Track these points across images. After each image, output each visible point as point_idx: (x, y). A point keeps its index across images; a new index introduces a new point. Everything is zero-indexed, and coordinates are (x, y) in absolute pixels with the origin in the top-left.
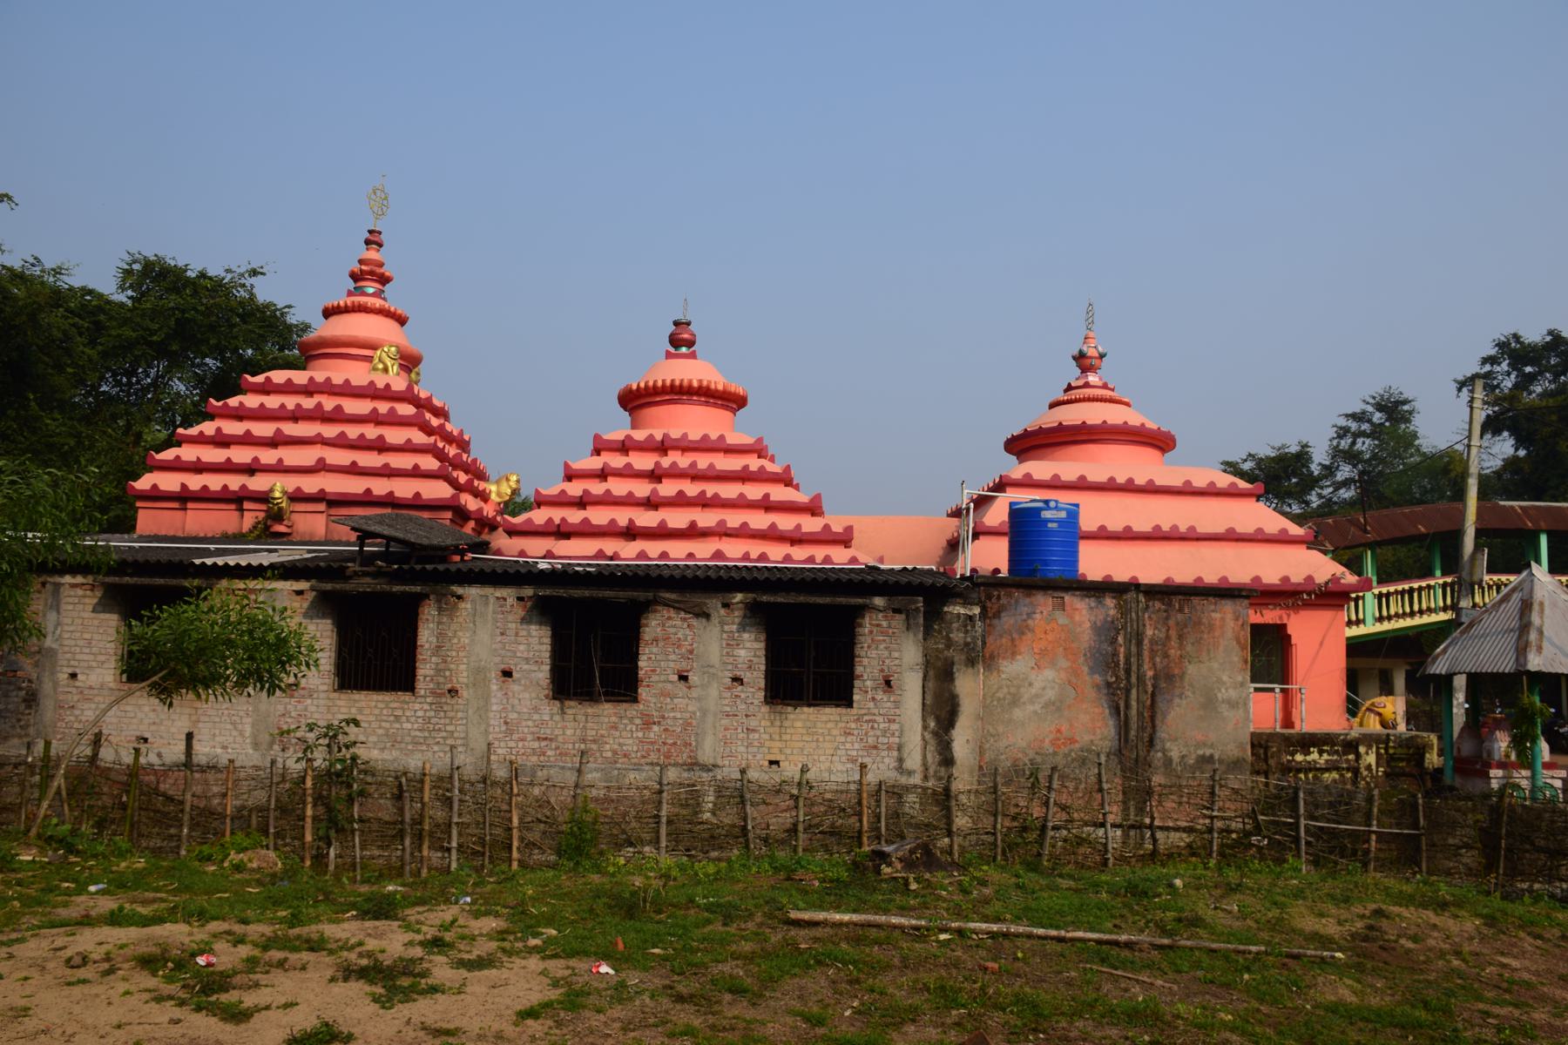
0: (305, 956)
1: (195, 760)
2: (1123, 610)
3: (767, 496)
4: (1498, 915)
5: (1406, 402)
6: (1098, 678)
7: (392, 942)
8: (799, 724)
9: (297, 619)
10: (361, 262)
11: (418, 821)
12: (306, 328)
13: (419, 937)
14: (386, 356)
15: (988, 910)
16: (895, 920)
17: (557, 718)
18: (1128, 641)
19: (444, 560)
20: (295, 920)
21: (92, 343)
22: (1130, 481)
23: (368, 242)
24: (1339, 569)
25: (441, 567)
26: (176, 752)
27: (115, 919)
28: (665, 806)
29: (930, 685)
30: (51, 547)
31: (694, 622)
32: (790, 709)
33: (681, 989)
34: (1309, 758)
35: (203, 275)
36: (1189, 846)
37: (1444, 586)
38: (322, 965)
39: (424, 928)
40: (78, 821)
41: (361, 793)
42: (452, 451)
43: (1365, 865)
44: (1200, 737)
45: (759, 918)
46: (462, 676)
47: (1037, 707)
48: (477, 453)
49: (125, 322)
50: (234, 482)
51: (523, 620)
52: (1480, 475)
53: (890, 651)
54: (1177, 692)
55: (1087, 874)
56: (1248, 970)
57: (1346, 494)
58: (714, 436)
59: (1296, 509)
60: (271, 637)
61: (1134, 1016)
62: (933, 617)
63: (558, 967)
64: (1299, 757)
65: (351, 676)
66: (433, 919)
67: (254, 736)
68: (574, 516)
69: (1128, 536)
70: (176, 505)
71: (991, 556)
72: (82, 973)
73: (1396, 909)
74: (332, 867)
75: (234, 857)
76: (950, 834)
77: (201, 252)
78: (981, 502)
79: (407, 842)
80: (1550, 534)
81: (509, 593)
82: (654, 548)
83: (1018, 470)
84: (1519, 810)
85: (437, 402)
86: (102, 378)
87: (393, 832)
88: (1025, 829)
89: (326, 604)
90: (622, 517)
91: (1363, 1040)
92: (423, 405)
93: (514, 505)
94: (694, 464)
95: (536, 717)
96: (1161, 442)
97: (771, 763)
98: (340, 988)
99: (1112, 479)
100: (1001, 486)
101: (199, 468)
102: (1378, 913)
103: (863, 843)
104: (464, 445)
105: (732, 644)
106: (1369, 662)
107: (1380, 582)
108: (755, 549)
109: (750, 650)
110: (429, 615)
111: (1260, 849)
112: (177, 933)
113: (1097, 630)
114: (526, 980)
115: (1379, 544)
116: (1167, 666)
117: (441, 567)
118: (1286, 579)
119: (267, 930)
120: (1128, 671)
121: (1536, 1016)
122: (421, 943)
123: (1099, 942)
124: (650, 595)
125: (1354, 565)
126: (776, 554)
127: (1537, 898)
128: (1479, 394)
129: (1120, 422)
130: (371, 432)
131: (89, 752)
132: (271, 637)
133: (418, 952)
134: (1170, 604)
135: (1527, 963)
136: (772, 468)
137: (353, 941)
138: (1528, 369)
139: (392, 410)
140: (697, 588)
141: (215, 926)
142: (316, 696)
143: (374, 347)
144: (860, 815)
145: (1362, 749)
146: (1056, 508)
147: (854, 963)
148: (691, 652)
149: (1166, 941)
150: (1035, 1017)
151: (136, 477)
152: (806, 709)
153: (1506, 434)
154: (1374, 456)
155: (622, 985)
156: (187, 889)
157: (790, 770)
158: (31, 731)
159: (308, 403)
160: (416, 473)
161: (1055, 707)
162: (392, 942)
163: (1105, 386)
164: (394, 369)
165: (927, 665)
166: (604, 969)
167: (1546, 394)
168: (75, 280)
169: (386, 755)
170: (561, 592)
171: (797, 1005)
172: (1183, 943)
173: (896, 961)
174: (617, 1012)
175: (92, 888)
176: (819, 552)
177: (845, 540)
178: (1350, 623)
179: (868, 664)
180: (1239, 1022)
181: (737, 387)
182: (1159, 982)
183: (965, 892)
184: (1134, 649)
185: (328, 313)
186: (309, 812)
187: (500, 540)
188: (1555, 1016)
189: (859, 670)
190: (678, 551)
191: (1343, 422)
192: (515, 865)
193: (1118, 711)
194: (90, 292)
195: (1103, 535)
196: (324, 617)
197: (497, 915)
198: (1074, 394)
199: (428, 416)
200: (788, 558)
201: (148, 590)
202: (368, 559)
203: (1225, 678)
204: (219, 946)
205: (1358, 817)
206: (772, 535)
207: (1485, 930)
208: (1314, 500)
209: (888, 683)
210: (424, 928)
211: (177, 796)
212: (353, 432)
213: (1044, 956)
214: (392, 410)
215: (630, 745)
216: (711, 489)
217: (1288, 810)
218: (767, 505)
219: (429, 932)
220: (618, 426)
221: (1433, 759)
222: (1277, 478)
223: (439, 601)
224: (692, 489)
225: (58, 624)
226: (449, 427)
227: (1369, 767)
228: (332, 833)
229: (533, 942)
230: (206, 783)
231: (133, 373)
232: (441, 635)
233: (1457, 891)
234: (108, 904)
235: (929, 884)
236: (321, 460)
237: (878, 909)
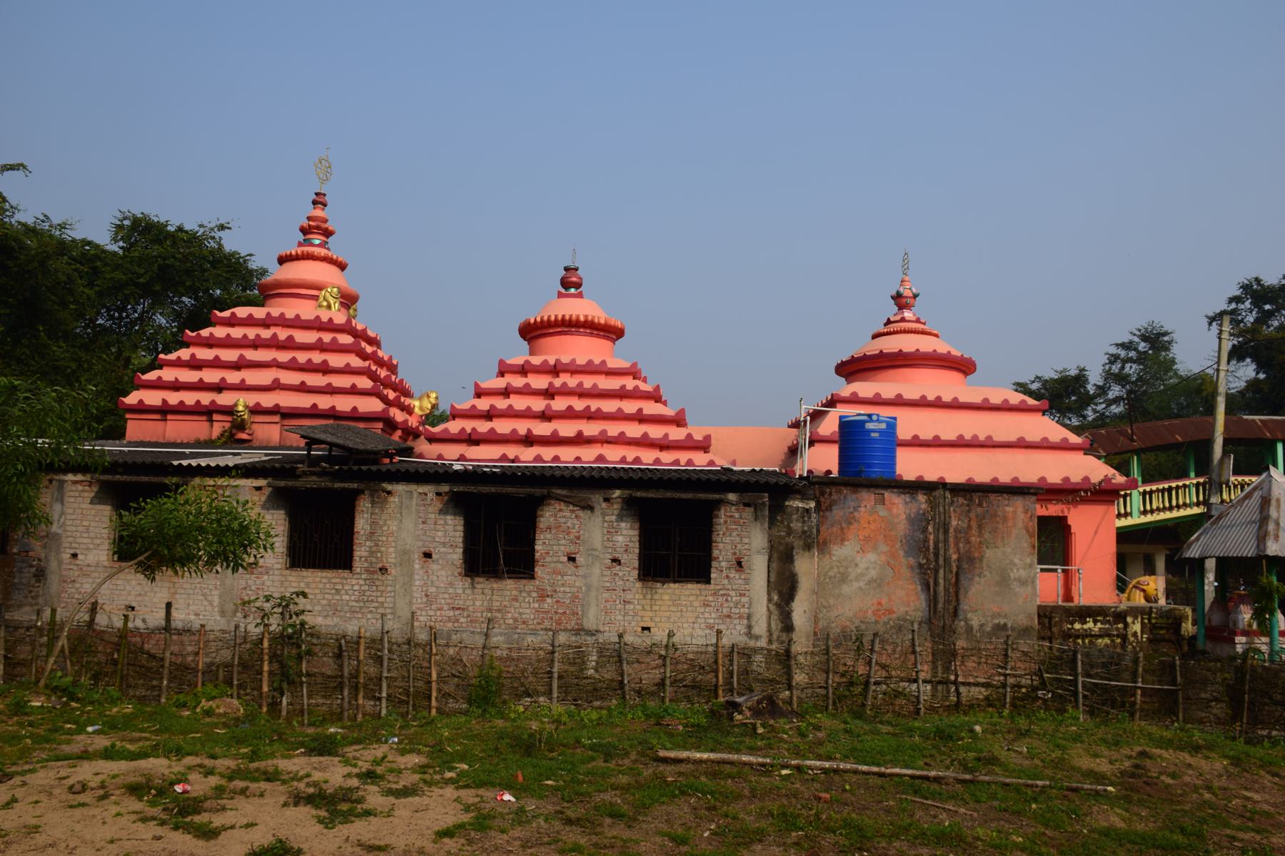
0: (263, 785)
1: (173, 625)
2: (933, 505)
3: (640, 410)
4: (1243, 756)
5: (1166, 334)
6: (912, 561)
7: (334, 774)
8: (666, 597)
10: (309, 218)
11: (355, 676)
12: (264, 272)
13: (356, 771)
14: (330, 295)
15: (822, 751)
16: (745, 758)
17: (468, 591)
18: (937, 530)
19: (376, 462)
20: (254, 756)
21: (91, 285)
22: (939, 398)
23: (315, 203)
24: (1110, 471)
25: (374, 468)
26: (157, 618)
27: (108, 754)
28: (556, 664)
29: (774, 565)
30: (57, 451)
31: (581, 513)
32: (659, 585)
33: (570, 813)
34: (1085, 627)
35: (180, 229)
36: (987, 698)
37: (1197, 485)
38: (277, 793)
39: (360, 763)
41: (309, 653)
42: (383, 373)
43: (1132, 715)
44: (996, 609)
45: (633, 756)
47: (862, 584)
48: (403, 374)
49: (117, 267)
50: (206, 398)
51: (441, 512)
52: (1227, 394)
53: (741, 538)
54: (977, 571)
56: (1035, 800)
57: (1116, 409)
58: (597, 361)
59: (1075, 422)
60: (235, 525)
61: (942, 838)
62: (776, 510)
63: (469, 796)
64: (1077, 626)
66: (367, 756)
67: (221, 606)
68: (483, 427)
70: (158, 417)
72: (82, 798)
73: (1158, 751)
74: (284, 713)
75: (205, 704)
76: (790, 688)
77: (180, 211)
78: (816, 416)
79: (346, 693)
81: (429, 490)
82: (548, 453)
84: (1260, 670)
85: (371, 333)
86: (98, 313)
87: (334, 684)
88: (851, 684)
89: (280, 498)
90: (522, 427)
92: (360, 335)
93: (433, 417)
94: (580, 384)
95: (451, 590)
96: (964, 367)
97: (644, 629)
98: (292, 812)
99: (924, 397)
100: (832, 402)
101: (176, 386)
102: (1143, 754)
103: (720, 695)
104: (392, 368)
105: (612, 531)
106: (1135, 548)
108: (631, 453)
109: (627, 537)
110: (364, 504)
111: (1045, 701)
112: (158, 766)
113: (911, 520)
114: (443, 806)
116: (969, 551)
117: (374, 468)
118: (1066, 479)
119: (231, 763)
120: (936, 555)
121: (1274, 840)
122: (358, 776)
124: (545, 491)
125: (1123, 468)
126: (648, 457)
128: (1227, 327)
129: (930, 350)
130: (317, 357)
131: (87, 618)
132: (235, 525)
133: (355, 782)
134: (971, 500)
135: (1267, 797)
137: (301, 773)
138: (1267, 307)
139: (334, 339)
140: (583, 486)
141: (190, 760)
142: (273, 572)
143: (320, 288)
144: (716, 671)
145: (1129, 620)
146: (878, 420)
147: (712, 793)
148: (578, 538)
149: (968, 777)
150: (861, 838)
151: (126, 394)
152: (672, 585)
153: (1248, 360)
154: (1140, 379)
155: (521, 811)
156: (166, 730)
157: (659, 635)
159: (266, 334)
160: (354, 391)
161: (876, 583)
162: (334, 774)
163: (918, 321)
164: (336, 306)
165: (772, 548)
166: (507, 797)
169: (329, 622)
172: (982, 778)
173: (746, 792)
174: (517, 832)
175: (90, 729)
176: (683, 457)
177: (704, 446)
178: (1119, 516)
179: (723, 549)
180: (1028, 844)
181: (616, 321)
182: (962, 810)
183: (803, 735)
184: (941, 537)
185: (282, 260)
186: (266, 668)
187: (422, 446)
189: (715, 553)
190: (567, 455)
191: (1114, 350)
192: (434, 712)
193: (928, 587)
194: (89, 243)
195: (916, 443)
196: (278, 508)
197: (419, 753)
198: (892, 327)
199: (363, 344)
200: (657, 461)
201: (135, 485)
202: (314, 461)
203: (1016, 561)
204: (193, 777)
205: (1126, 675)
208: (1090, 414)
209: (739, 564)
210: (360, 763)
212: (302, 357)
213: (868, 788)
214: (334, 339)
215: (528, 614)
216: (595, 404)
217: (1067, 669)
218: (640, 418)
219: (364, 766)
220: (519, 353)
221: (1188, 628)
223: (372, 496)
224: (579, 405)
225: (63, 513)
226: (380, 353)
227: (1135, 634)
228: (285, 685)
229: (449, 775)
230: (182, 643)
231: (124, 309)
232: (374, 523)
234: (102, 742)
235: (773, 729)
236: (276, 381)
237: (731, 749)
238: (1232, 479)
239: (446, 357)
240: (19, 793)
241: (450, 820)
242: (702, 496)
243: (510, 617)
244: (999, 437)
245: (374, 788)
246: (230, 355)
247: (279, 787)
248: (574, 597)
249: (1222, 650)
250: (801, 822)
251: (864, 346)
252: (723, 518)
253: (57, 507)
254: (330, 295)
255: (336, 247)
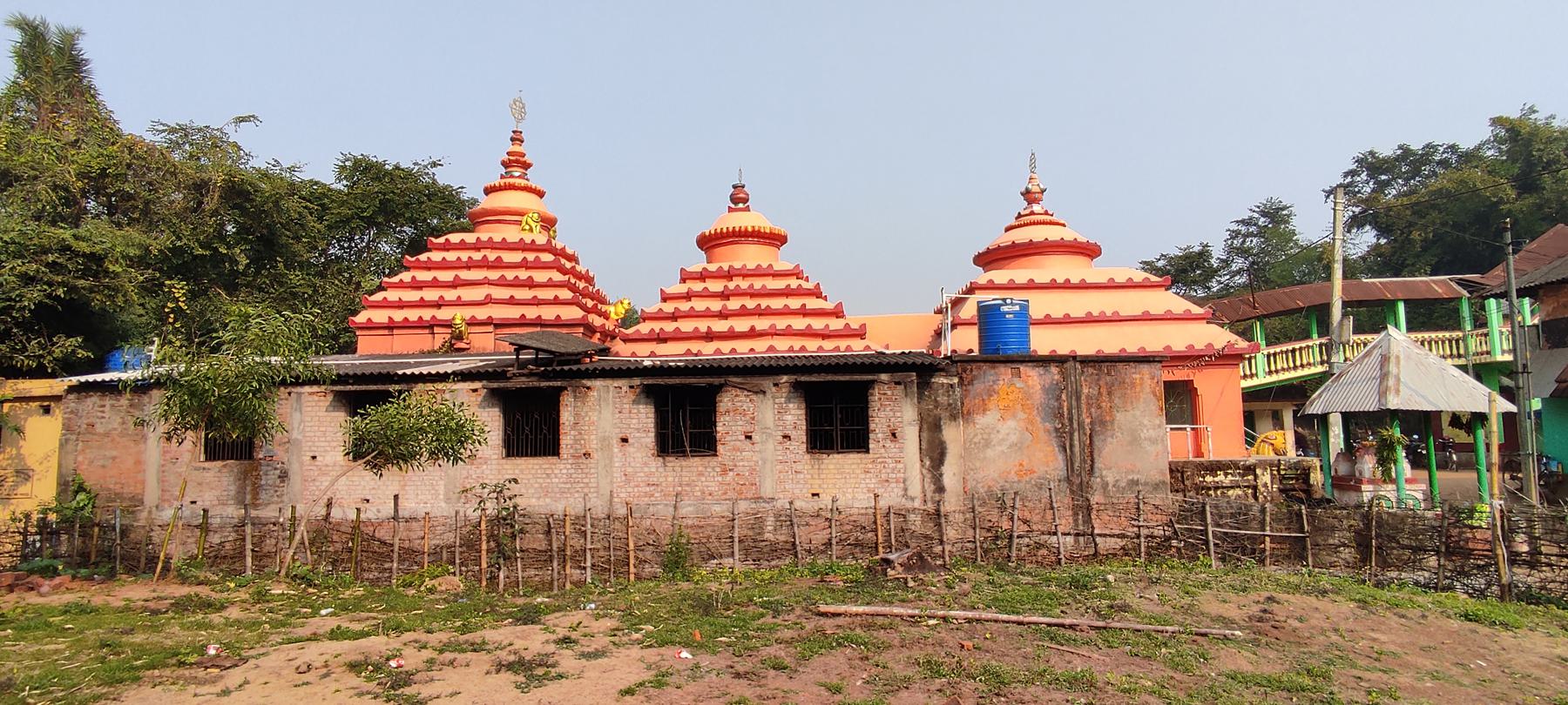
0: (469, 655)
7: (533, 641)
9: (472, 410)
11: (562, 550)
12: (475, 202)
13: (554, 637)
14: (531, 220)
16: (896, 610)
18: (1069, 398)
19: (578, 362)
20: (465, 629)
21: (321, 219)
22: (1068, 281)
23: (512, 139)
24: (1234, 338)
25: (575, 368)
26: (388, 510)
27: (336, 635)
29: (925, 435)
30: (288, 368)
31: (754, 397)
33: (740, 668)
35: (397, 168)
36: (1123, 548)
37: (1321, 345)
38: (483, 660)
40: (316, 563)
41: (521, 531)
42: (581, 285)
43: (1262, 561)
45: (798, 611)
46: (593, 444)
47: (1004, 448)
48: (600, 285)
49: (343, 203)
50: (427, 314)
52: (1345, 260)
53: (894, 413)
55: (1042, 571)
56: (1165, 644)
57: (1241, 280)
59: (1201, 293)
61: (1073, 682)
62: (924, 385)
63: (652, 655)
64: (1209, 479)
65: (517, 445)
66: (562, 623)
67: (446, 494)
68: (669, 327)
69: (1067, 321)
71: (965, 341)
72: (305, 678)
73: (1286, 596)
75: (428, 583)
76: (942, 542)
77: (395, 153)
79: (555, 564)
80: (1406, 302)
81: (623, 383)
83: (983, 277)
84: (1385, 517)
85: (569, 251)
87: (544, 558)
88: (997, 538)
90: (703, 325)
91: (1256, 700)
92: (561, 253)
93: (629, 319)
94: (751, 286)
96: (1089, 251)
97: (785, 437)
98: (495, 679)
100: (971, 290)
101: (401, 305)
102: (1270, 599)
103: (882, 556)
104: (589, 280)
105: (781, 412)
106: (1261, 405)
107: (1457, 326)
108: (797, 343)
109: (795, 416)
110: (567, 400)
111: (1179, 549)
112: (378, 644)
114: (629, 665)
115: (1266, 316)
117: (575, 368)
119: (444, 637)
122: (556, 642)
123: (1049, 625)
125: (1246, 334)
126: (812, 346)
127: (1402, 586)
130: (523, 274)
131: (324, 512)
132: (453, 424)
133: (552, 648)
135: (1393, 637)
136: (805, 285)
137: (505, 643)
140: (755, 373)
141: (408, 636)
142: (488, 460)
143: (522, 214)
144: (876, 530)
145: (1258, 471)
147: (865, 644)
149: (1101, 624)
150: (999, 683)
151: (355, 313)
153: (1368, 227)
155: (697, 666)
156: (393, 609)
157: (825, 501)
158: (285, 498)
159: (477, 256)
160: (556, 301)
161: (1017, 447)
162: (533, 641)
163: (1046, 213)
164: (537, 228)
165: (922, 420)
166: (685, 654)
167: (1399, 195)
168: (306, 176)
169: (541, 502)
170: (660, 381)
171: (822, 678)
172: (1114, 624)
173: (896, 642)
174: (691, 687)
175: (323, 612)
176: (843, 344)
178: (1245, 377)
179: (879, 422)
180: (1156, 688)
181: (780, 228)
182: (1096, 656)
185: (489, 191)
186: (484, 547)
187: (618, 346)
188: (1418, 679)
189: (872, 426)
190: (743, 347)
191: (1234, 227)
192: (632, 577)
194: (316, 183)
195: (1048, 321)
197: (612, 617)
199: (563, 261)
200: (820, 349)
201: (361, 394)
202: (522, 365)
204: (407, 651)
205: (1254, 524)
206: (809, 333)
207: (1358, 612)
208: (1215, 286)
209: (894, 435)
210: (558, 630)
211: (387, 538)
212: (510, 275)
213: (1008, 635)
215: (713, 487)
217: (1198, 526)
218: (804, 312)
219: (561, 632)
220: (697, 261)
221: (1317, 478)
222: (1185, 271)
224: (751, 304)
226: (578, 268)
227: (1265, 485)
228: (501, 561)
229: (636, 636)
231: (351, 240)
233: (1335, 580)
234: (333, 623)
235: (923, 583)
237: (886, 602)
238: (1356, 338)
239: (636, 263)
240: (251, 676)
241: (632, 679)
242: (857, 377)
243: (692, 492)
244: (1154, 311)
245: (569, 652)
246: (446, 276)
247: (483, 656)
248: (752, 471)
249: (1350, 498)
250: (945, 669)
251: (998, 237)
252: (876, 396)
253: (297, 415)
254: (531, 220)
255: (534, 178)
